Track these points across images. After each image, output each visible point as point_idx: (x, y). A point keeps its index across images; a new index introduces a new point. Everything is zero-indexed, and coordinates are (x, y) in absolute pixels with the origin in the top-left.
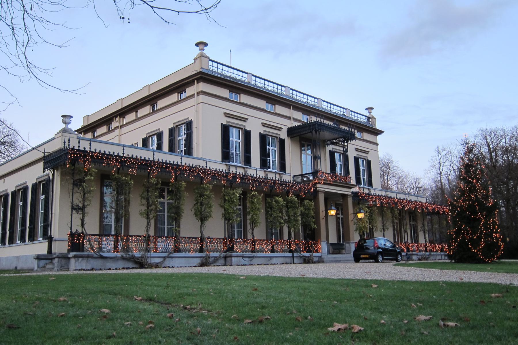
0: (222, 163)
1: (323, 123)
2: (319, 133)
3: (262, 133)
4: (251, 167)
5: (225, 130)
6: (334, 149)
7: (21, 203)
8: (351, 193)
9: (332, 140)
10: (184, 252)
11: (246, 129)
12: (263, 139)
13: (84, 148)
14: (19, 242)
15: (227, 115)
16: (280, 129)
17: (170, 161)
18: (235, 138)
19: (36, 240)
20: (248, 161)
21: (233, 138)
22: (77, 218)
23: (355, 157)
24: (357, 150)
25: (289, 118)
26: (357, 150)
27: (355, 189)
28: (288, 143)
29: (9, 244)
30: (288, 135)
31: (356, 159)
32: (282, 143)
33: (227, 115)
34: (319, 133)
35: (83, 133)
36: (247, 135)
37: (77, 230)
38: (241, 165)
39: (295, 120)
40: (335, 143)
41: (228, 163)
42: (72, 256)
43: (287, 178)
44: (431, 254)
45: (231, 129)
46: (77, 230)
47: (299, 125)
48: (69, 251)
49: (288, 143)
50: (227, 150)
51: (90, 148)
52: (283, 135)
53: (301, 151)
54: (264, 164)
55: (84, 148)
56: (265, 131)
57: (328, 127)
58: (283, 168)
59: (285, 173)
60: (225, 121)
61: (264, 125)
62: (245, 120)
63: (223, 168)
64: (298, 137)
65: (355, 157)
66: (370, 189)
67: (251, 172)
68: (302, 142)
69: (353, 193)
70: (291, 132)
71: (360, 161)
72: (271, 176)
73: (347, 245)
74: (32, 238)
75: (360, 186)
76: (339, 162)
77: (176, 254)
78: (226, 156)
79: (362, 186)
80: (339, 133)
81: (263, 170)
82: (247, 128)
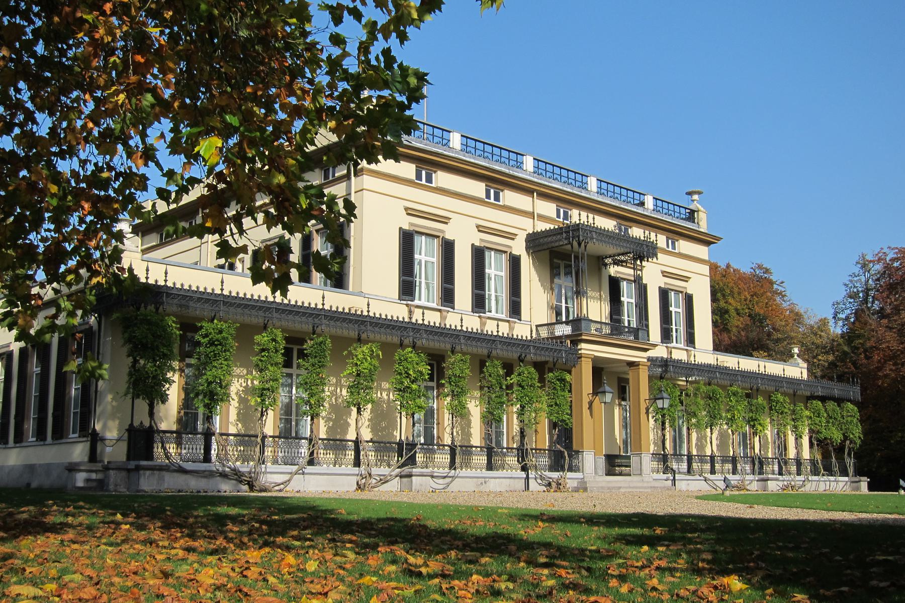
0: (399, 301)
1: (594, 227)
2: (585, 246)
3: (663, 286)
4: (454, 309)
5: (407, 240)
6: (618, 272)
7: (37, 370)
8: (646, 360)
9: (614, 256)
10: (364, 39)
11: (447, 237)
12: (479, 255)
13: (156, 281)
14: (34, 439)
15: (410, 212)
16: (512, 237)
17: (303, 303)
18: (677, 309)
19: (67, 438)
20: (448, 297)
21: (420, 254)
22: (142, 405)
23: (660, 288)
24: (665, 274)
25: (531, 215)
26: (665, 274)
27: (660, 352)
28: (527, 266)
29: (15, 442)
30: (527, 248)
31: (664, 294)
32: (515, 262)
33: (410, 212)
34: (585, 246)
35: (140, 234)
36: (448, 248)
37: (141, 423)
38: (682, 346)
39: (542, 218)
40: (622, 261)
41: (409, 302)
42: (133, 467)
43: (522, 331)
44: (808, 478)
45: (417, 239)
46: (141, 423)
47: (552, 228)
48: (129, 458)
49: (527, 266)
50: (410, 279)
51: (166, 281)
52: (519, 247)
53: (552, 282)
54: (479, 303)
55: (156, 281)
56: (481, 240)
57: (602, 234)
58: (515, 309)
59: (520, 320)
60: (407, 222)
61: (480, 229)
62: (445, 220)
63: (398, 311)
64: (548, 251)
65: (660, 288)
66: (691, 351)
67: (452, 321)
68: (555, 261)
69: (649, 359)
70: (535, 242)
71: (672, 295)
72: (491, 328)
73: (634, 460)
74: (59, 434)
75: (668, 345)
76: (628, 298)
77: (310, 469)
78: (407, 289)
79: (416, 302)
80: (625, 245)
81: (477, 315)
82: (449, 236)
